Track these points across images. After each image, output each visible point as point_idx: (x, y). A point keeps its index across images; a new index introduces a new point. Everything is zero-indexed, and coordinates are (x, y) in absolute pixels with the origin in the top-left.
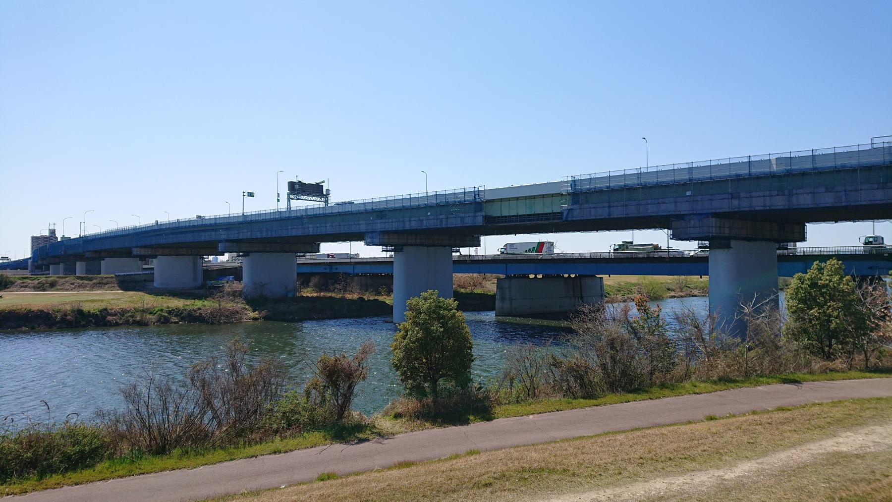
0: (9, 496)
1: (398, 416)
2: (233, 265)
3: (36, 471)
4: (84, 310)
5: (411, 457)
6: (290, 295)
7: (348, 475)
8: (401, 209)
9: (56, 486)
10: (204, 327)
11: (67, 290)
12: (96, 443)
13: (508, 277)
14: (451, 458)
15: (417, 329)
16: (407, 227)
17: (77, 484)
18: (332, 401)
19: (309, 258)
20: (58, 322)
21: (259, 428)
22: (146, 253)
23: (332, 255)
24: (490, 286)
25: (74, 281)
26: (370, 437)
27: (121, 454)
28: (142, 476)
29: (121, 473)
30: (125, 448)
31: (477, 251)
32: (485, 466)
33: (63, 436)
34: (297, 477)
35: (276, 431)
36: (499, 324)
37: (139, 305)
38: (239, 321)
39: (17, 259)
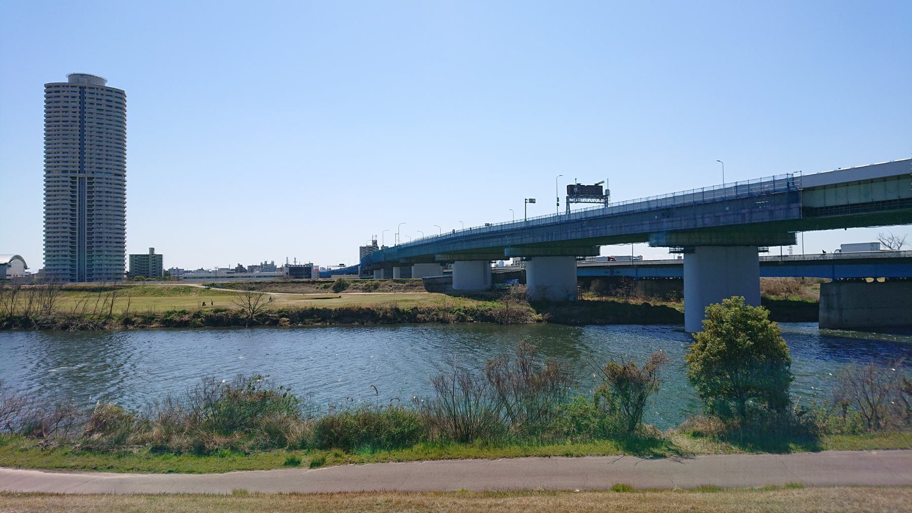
0: (352, 464)
1: (696, 435)
2: (518, 268)
3: (369, 446)
4: (400, 308)
5: (717, 481)
6: (571, 299)
7: (644, 490)
8: (692, 206)
9: (384, 461)
10: (494, 326)
11: (386, 291)
12: (413, 426)
13: (835, 281)
14: (766, 489)
15: (718, 339)
16: (700, 224)
17: (399, 461)
18: (622, 411)
19: (588, 261)
20: (380, 319)
21: (550, 429)
22: (446, 259)
23: (612, 258)
24: (811, 292)
25: (392, 284)
26: (667, 454)
27: (433, 438)
28: (450, 461)
29: (433, 455)
30: (436, 433)
31: (791, 250)
32: (813, 503)
33: (388, 417)
34: (591, 483)
35: (567, 434)
36: (824, 338)
37: (441, 305)
38: (524, 323)
39: (350, 266)
